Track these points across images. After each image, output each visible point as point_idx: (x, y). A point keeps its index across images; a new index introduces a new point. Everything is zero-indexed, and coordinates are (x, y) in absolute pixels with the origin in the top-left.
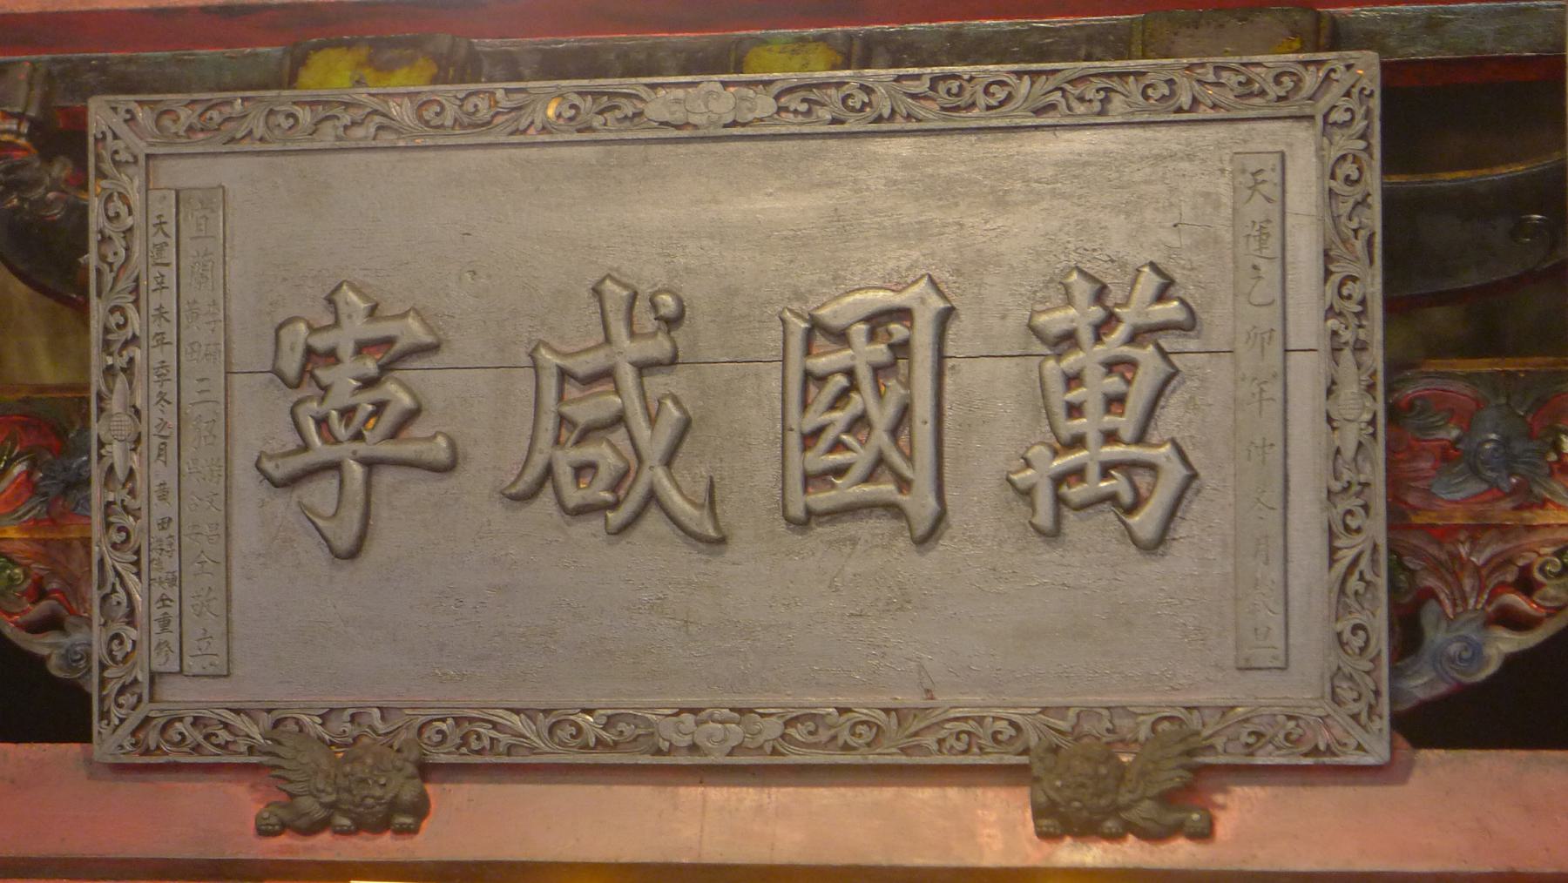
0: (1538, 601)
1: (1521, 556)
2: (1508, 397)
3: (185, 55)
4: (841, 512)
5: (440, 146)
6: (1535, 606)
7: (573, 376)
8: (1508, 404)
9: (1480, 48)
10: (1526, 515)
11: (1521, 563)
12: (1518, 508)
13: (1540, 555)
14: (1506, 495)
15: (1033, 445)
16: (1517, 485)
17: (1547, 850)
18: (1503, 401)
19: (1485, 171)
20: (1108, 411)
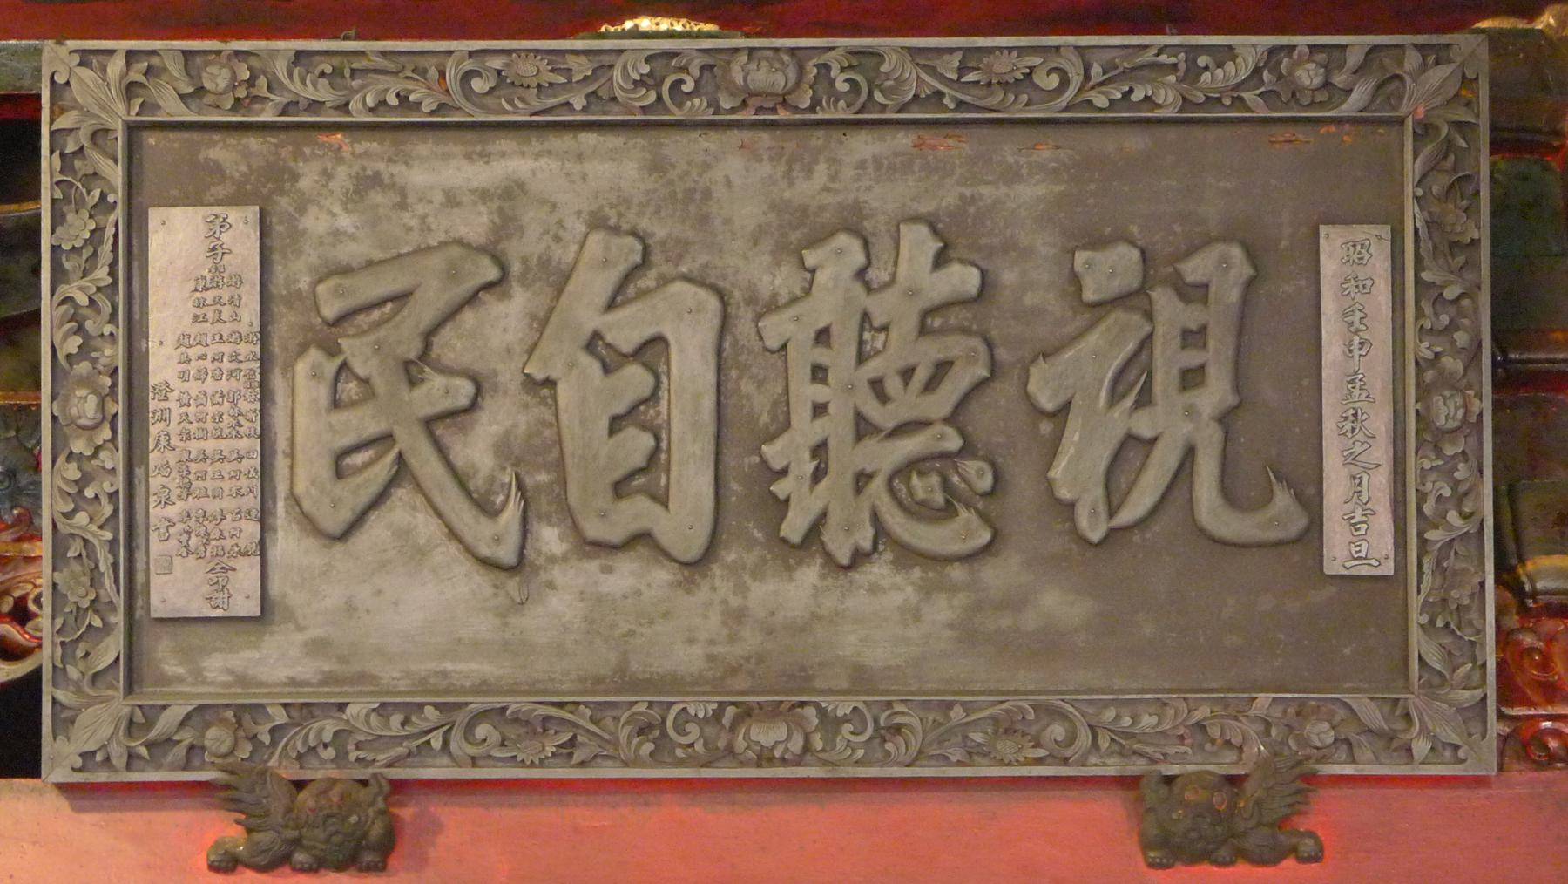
0: (31, 632)
1: (18, 588)
2: (18, 431)
3: (710, 36)
4: (130, 567)
5: (977, 107)
6: (27, 636)
7: (1191, 332)
8: (17, 436)
9: (18, 84)
10: (26, 546)
11: (17, 594)
12: (19, 540)
13: (35, 586)
14: (9, 527)
15: (1028, 398)
16: (19, 515)
17: (11, 877)
18: (13, 433)
19: (14, 207)
20: (1185, 346)
